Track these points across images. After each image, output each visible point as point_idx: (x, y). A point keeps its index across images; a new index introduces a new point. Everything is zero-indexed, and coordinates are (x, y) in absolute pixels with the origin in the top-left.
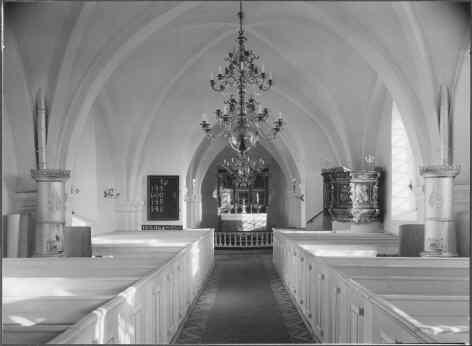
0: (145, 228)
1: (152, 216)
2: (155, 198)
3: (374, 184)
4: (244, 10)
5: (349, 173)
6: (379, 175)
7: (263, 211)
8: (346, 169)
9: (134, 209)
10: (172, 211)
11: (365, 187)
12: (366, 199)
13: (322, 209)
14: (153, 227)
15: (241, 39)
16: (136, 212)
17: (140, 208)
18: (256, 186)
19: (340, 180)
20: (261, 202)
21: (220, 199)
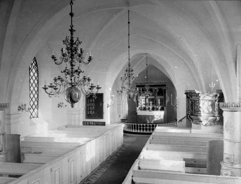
0: (85, 123)
1: (88, 116)
2: (90, 106)
3: (216, 101)
4: (130, 22)
5: (199, 93)
6: (218, 95)
7: (162, 109)
8: (197, 92)
9: (77, 113)
10: (99, 113)
11: (210, 103)
12: (211, 110)
13: (185, 115)
14: (89, 124)
15: (72, 31)
16: (79, 114)
17: (82, 112)
18: (159, 94)
19: (194, 98)
20: (161, 104)
21: (138, 102)
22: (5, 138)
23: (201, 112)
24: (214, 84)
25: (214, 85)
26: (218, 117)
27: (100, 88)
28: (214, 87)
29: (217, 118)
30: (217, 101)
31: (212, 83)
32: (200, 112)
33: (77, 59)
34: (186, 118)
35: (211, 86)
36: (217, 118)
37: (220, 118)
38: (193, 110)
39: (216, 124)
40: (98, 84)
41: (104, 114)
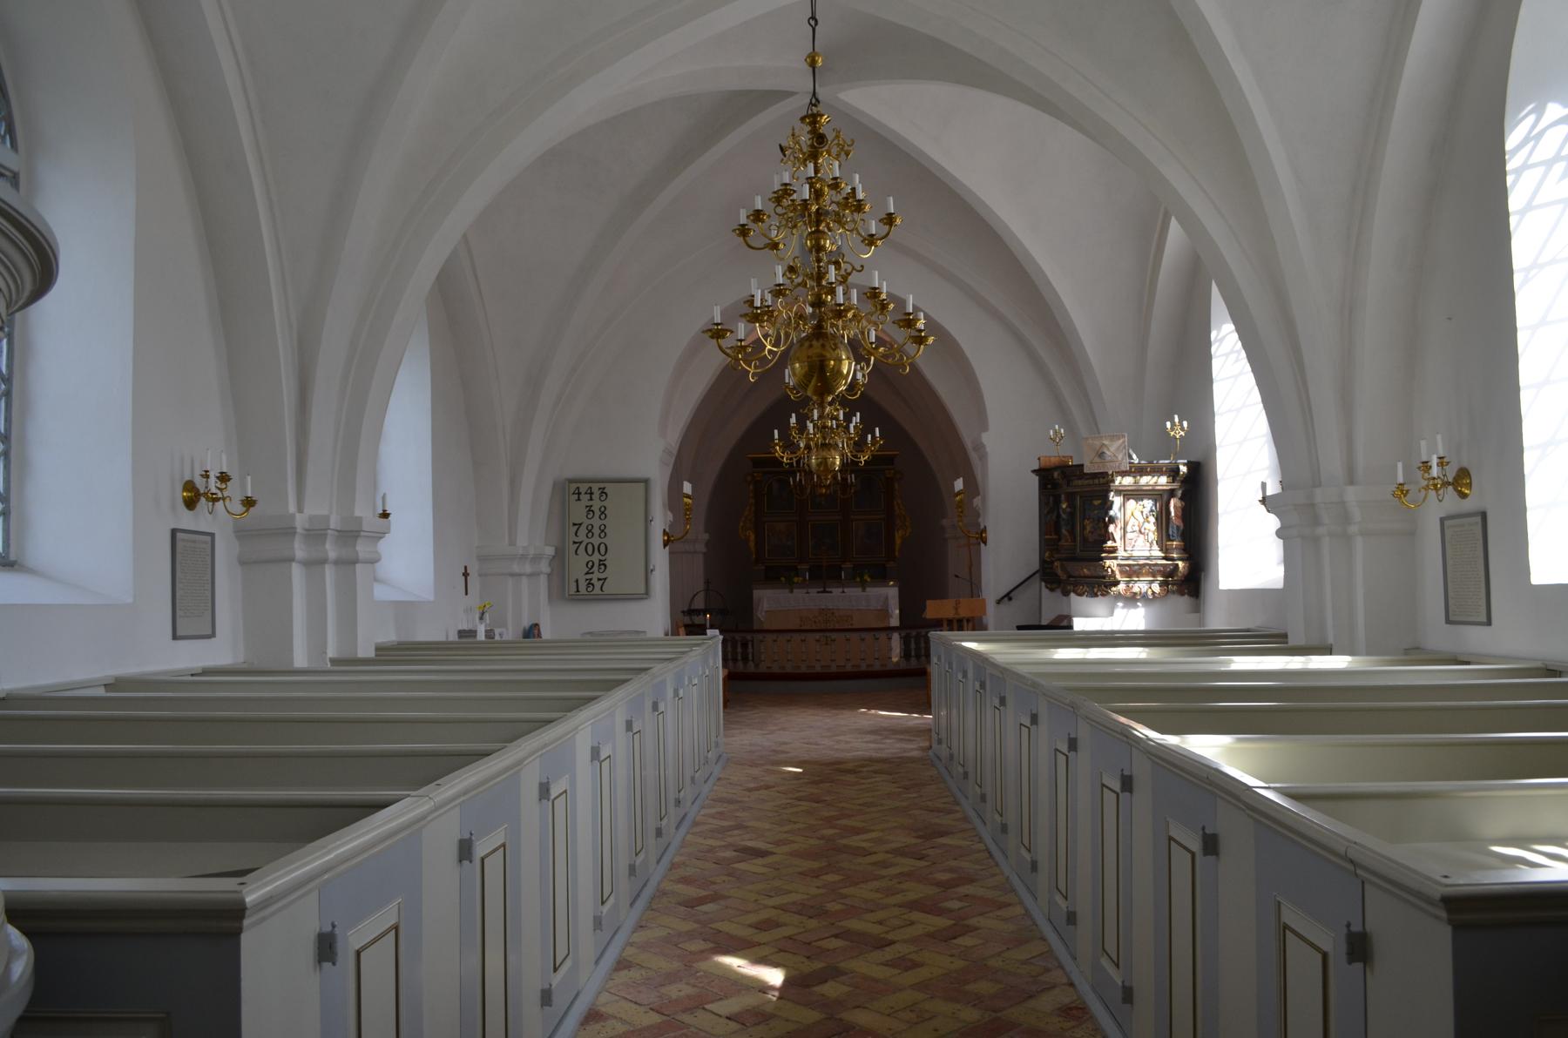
13: (1036, 566)
22: (720, 847)
23: (1114, 540)
24: (1185, 424)
25: (1182, 429)
26: (1180, 559)
27: (189, 486)
28: (1182, 433)
29: (1181, 564)
30: (1179, 493)
31: (1177, 420)
32: (1110, 543)
33: (801, 236)
34: (1037, 575)
35: (1172, 429)
36: (1181, 564)
37: (1190, 564)
38: (1074, 540)
39: (1173, 592)
40: (221, 467)
41: (1531, 576)
